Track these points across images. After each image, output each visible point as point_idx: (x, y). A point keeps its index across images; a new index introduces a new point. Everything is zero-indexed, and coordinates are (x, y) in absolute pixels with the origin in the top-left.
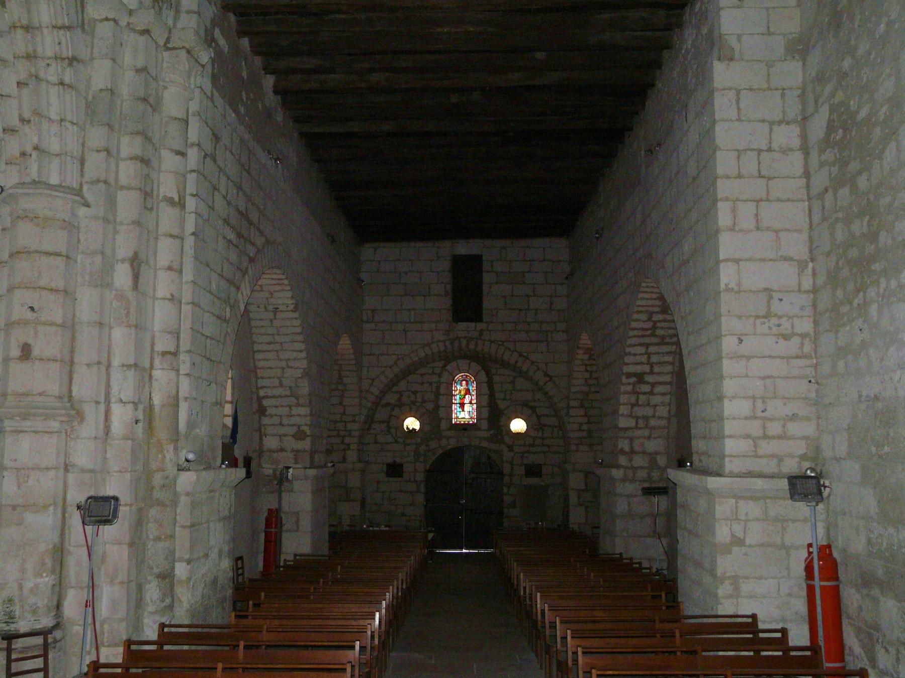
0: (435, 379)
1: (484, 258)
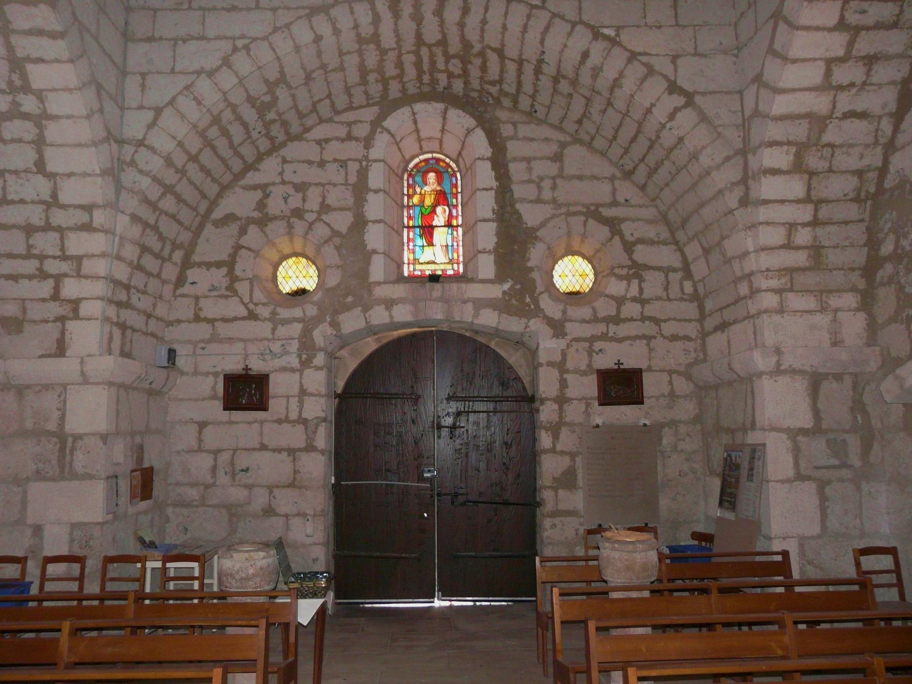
0: (354, 150)
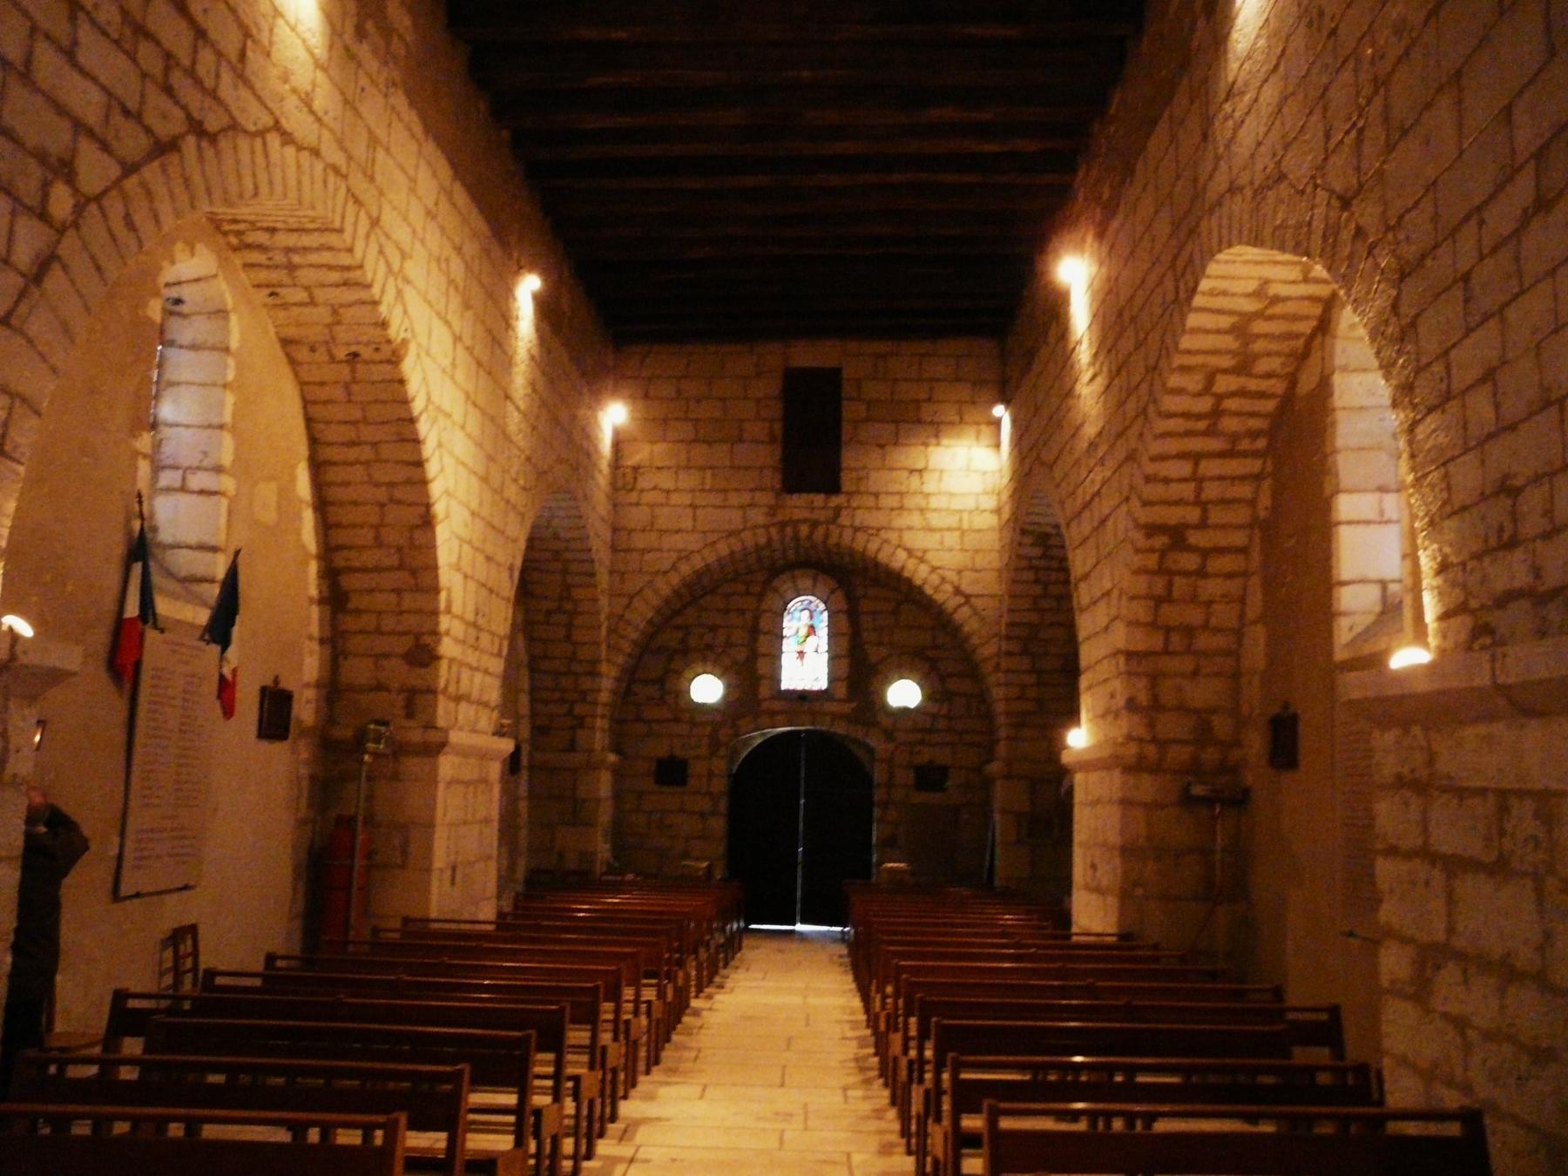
1: (845, 375)
